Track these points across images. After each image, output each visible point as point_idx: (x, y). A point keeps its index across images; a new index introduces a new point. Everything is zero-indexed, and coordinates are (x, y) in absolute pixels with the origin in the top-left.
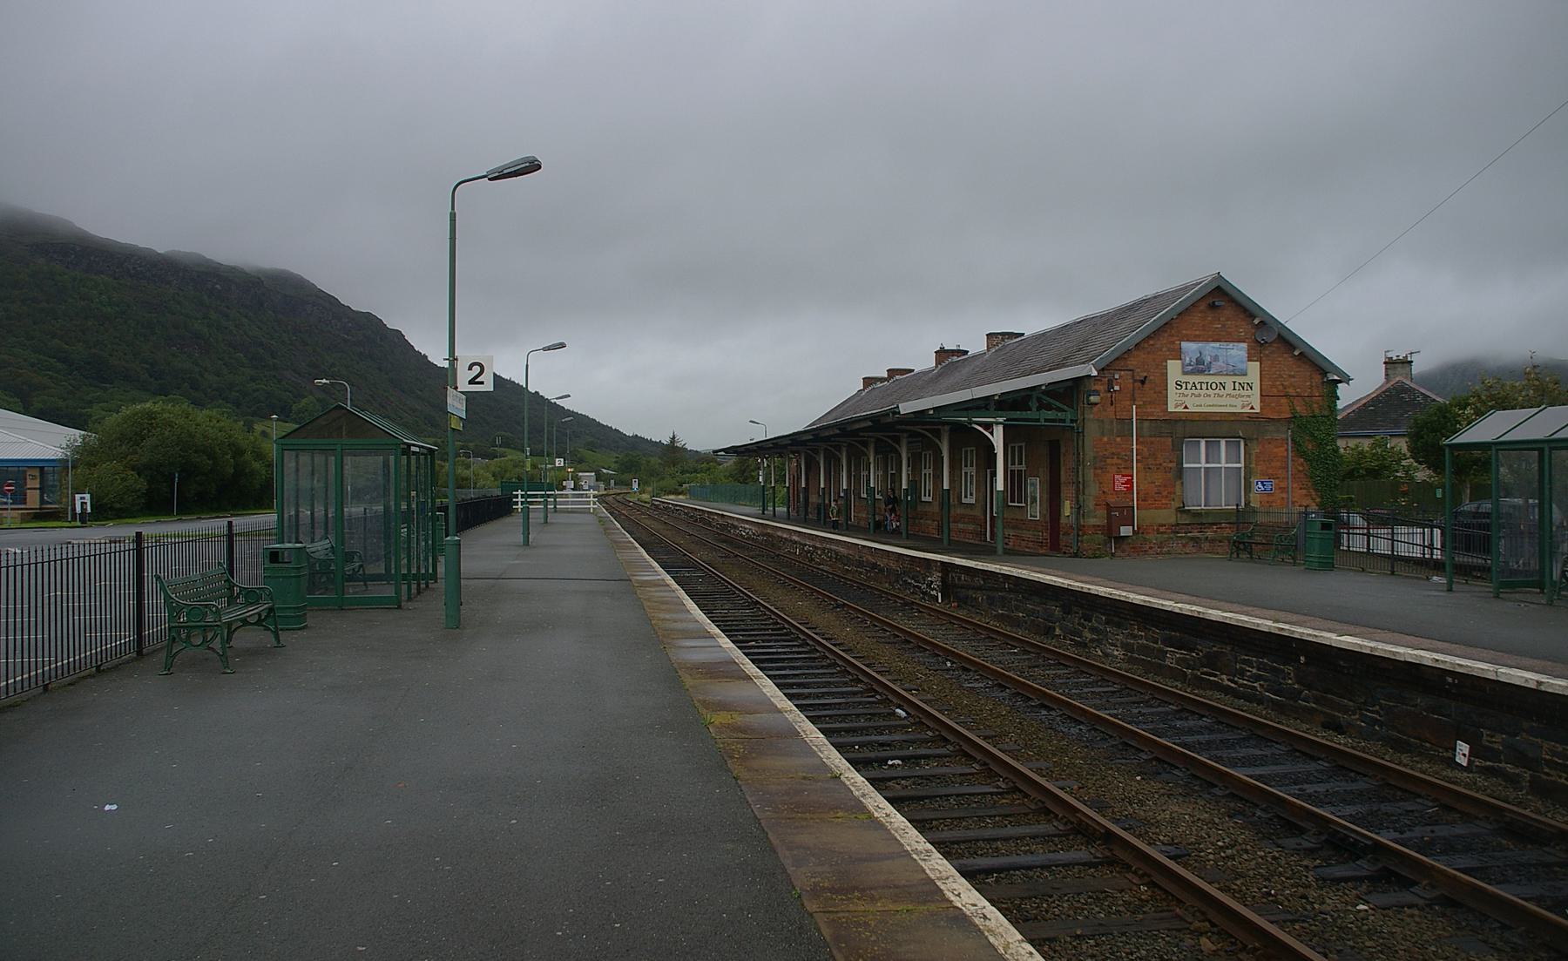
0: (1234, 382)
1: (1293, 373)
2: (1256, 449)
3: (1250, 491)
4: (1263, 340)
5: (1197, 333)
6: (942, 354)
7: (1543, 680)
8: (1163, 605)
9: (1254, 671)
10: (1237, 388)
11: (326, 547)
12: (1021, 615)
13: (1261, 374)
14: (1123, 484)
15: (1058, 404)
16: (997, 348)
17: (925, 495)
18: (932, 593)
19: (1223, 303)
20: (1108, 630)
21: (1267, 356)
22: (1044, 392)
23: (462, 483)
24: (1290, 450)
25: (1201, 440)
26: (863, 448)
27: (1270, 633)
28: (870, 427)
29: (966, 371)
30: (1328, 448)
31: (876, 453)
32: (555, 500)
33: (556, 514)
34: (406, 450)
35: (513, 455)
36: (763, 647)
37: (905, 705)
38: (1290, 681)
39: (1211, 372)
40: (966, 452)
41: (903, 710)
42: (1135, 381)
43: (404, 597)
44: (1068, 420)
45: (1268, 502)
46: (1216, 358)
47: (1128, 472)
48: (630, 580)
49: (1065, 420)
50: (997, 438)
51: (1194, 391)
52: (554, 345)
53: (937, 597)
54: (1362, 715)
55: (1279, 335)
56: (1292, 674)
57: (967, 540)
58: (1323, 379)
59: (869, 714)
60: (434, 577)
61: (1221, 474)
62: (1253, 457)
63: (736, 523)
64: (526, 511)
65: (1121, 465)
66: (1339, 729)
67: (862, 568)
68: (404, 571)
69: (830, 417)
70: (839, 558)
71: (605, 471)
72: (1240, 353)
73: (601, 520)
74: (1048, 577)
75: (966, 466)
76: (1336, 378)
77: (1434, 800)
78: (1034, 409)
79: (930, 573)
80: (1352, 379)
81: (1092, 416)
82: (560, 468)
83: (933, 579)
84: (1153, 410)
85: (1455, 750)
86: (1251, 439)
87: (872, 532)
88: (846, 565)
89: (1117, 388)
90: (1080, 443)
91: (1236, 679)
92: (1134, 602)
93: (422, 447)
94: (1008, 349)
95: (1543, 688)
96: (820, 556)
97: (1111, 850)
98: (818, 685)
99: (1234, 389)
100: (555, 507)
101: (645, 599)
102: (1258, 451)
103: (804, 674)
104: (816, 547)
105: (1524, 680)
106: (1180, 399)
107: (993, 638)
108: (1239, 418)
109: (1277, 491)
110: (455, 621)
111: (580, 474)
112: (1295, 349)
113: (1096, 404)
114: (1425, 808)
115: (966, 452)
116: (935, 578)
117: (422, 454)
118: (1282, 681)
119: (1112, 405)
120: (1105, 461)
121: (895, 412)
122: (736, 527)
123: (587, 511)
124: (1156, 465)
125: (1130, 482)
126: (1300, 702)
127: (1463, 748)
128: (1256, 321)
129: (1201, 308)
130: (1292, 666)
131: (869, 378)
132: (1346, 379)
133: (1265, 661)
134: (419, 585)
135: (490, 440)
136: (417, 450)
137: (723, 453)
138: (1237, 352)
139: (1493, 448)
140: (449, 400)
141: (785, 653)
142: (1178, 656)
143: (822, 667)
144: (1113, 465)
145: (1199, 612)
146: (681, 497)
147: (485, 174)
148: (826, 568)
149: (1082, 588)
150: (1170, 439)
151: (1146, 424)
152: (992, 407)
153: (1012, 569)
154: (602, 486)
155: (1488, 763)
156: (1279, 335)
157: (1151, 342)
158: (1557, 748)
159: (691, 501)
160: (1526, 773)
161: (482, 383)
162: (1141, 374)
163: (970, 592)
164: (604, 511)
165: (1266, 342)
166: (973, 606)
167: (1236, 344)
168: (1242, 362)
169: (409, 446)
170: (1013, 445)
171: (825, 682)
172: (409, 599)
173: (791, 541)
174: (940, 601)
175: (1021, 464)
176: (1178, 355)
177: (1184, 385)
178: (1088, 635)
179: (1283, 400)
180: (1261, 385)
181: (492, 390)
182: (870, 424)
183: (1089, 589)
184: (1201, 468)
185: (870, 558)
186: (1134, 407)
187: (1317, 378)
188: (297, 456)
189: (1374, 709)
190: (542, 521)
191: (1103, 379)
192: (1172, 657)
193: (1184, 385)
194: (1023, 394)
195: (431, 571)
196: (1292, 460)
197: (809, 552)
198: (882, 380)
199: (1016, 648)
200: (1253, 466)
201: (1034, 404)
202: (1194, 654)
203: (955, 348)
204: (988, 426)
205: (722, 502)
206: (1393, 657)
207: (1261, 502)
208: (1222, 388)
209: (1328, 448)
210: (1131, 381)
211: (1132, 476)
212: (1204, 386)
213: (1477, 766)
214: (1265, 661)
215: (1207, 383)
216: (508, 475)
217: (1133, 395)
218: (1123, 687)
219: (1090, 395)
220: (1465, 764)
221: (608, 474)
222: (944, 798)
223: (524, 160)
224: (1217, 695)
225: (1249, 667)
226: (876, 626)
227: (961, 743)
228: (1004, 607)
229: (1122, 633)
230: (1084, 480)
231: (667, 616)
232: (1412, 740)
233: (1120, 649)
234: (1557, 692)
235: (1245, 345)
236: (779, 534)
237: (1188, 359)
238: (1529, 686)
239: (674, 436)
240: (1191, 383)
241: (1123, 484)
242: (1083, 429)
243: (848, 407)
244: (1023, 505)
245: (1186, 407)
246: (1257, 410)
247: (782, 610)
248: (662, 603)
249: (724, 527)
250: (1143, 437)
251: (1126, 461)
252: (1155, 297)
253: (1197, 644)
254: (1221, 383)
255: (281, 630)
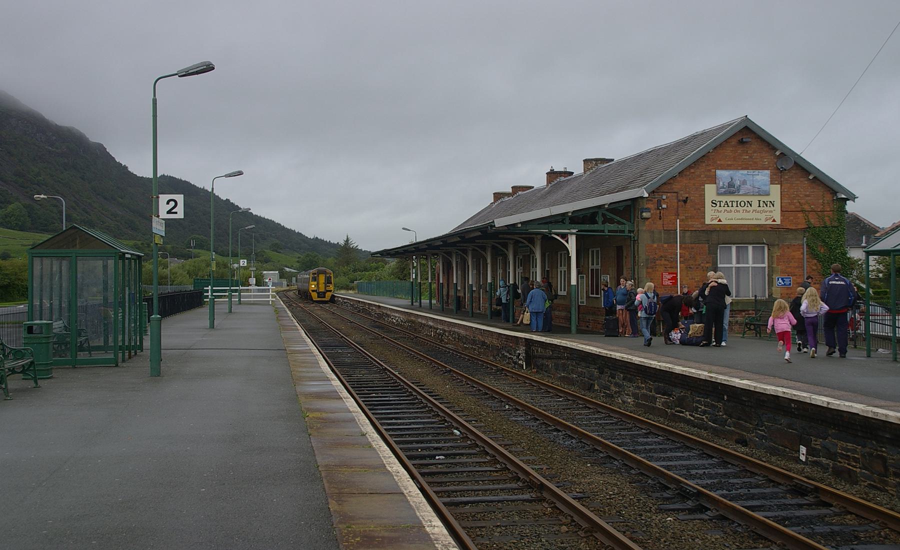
0: (759, 201)
1: (808, 193)
2: (777, 252)
3: (772, 286)
4: (782, 168)
5: (729, 163)
6: (552, 175)
7: (830, 401)
8: (651, 364)
9: (703, 408)
10: (761, 205)
11: (60, 326)
12: (575, 376)
13: (781, 194)
14: (669, 280)
15: (618, 218)
16: (591, 171)
17: (561, 290)
18: (519, 362)
19: (750, 140)
20: (625, 384)
21: (787, 180)
22: (607, 210)
23: (162, 280)
24: (805, 254)
25: (732, 245)
26: (482, 252)
27: (706, 380)
28: (480, 236)
29: (566, 189)
30: (837, 251)
31: (473, 258)
32: (240, 295)
33: (240, 306)
34: (122, 256)
35: (204, 255)
36: (381, 397)
37: (461, 428)
38: (721, 414)
39: (740, 193)
40: (561, 254)
41: (459, 431)
42: (679, 201)
43: (120, 360)
44: (626, 231)
45: (787, 294)
46: (744, 182)
47: (673, 271)
48: (286, 350)
49: (624, 231)
50: (572, 245)
51: (726, 208)
52: (235, 173)
53: (523, 365)
54: (756, 433)
55: (795, 163)
56: (722, 409)
57: (561, 324)
58: (833, 197)
59: (436, 433)
60: (141, 348)
61: (749, 273)
62: (775, 259)
63: (389, 313)
64: (213, 303)
65: (667, 265)
66: (743, 442)
67: (475, 345)
68: (120, 344)
69: (470, 223)
70: (460, 338)
71: (287, 269)
72: (764, 178)
73: (277, 311)
74: (588, 347)
75: (561, 266)
76: (843, 196)
77: (764, 477)
78: (600, 223)
79: (518, 347)
80: (857, 197)
81: (644, 228)
82: (244, 268)
83: (520, 352)
84: (694, 223)
85: (799, 452)
86: (773, 245)
87: (489, 319)
88: (465, 343)
89: (664, 206)
90: (636, 249)
91: (694, 414)
92: (635, 362)
93: (133, 254)
94: (598, 172)
95: (830, 406)
96: (448, 337)
97: (542, 493)
98: (409, 418)
99: (759, 206)
100: (240, 300)
101: (291, 361)
102: (779, 254)
103: (402, 412)
104: (445, 331)
105: (821, 402)
106: (714, 214)
107: (549, 392)
108: (763, 229)
109: (795, 286)
110: (156, 372)
111: (265, 272)
112: (810, 174)
113: (649, 219)
114: (758, 481)
115: (561, 254)
116: (521, 350)
117: (133, 259)
118: (717, 414)
119: (660, 219)
120: (655, 263)
121: (492, 225)
122: (388, 316)
123: (266, 303)
124: (696, 265)
125: (675, 278)
126: (726, 427)
127: (803, 449)
128: (778, 153)
129: (733, 143)
130: (722, 403)
131: (499, 193)
132: (853, 198)
133: (708, 400)
134: (130, 352)
135: (186, 242)
136: (129, 256)
137: (379, 255)
138: (762, 177)
139: (892, 254)
140: (154, 225)
141: (394, 400)
142: (663, 400)
143: (417, 408)
144: (661, 265)
145: (669, 368)
146: (351, 292)
147: (176, 72)
148: (450, 346)
149: (607, 354)
150: (707, 245)
151: (688, 234)
152: (567, 221)
153: (568, 343)
154: (285, 282)
155: (815, 458)
156: (795, 163)
157: (692, 171)
158: (843, 445)
159: (358, 295)
160: (830, 462)
161: (176, 213)
162: (683, 195)
163: (545, 362)
164: (282, 303)
165: (785, 170)
166: (546, 372)
167: (760, 171)
168: (766, 185)
169: (124, 254)
170: (593, 249)
171: (415, 416)
172: (123, 361)
173: (427, 326)
174: (524, 368)
175: (598, 265)
176: (713, 180)
177: (718, 204)
178: (613, 388)
179: (800, 215)
180: (781, 203)
181: (183, 217)
182: (480, 233)
183: (611, 355)
184: (749, 267)
185: (480, 337)
186: (678, 220)
187: (828, 197)
188: (42, 261)
189: (762, 428)
190: (228, 311)
191: (653, 200)
192: (660, 401)
193: (718, 204)
194: (591, 211)
195: (138, 344)
196: (808, 262)
197: (439, 334)
198: (508, 195)
199: (561, 397)
200: (774, 266)
201: (600, 219)
202: (671, 398)
203: (563, 170)
204: (564, 236)
205: (383, 296)
206: (764, 392)
207: (781, 294)
208: (749, 205)
209: (837, 251)
210: (676, 201)
211: (676, 274)
212: (735, 204)
213: (810, 461)
214: (708, 400)
215: (737, 202)
216: (200, 273)
217: (677, 212)
218: (620, 420)
219: (643, 212)
220: (804, 460)
221: (290, 272)
222: (460, 473)
223: (203, 64)
224: (687, 428)
225: (700, 405)
226: (469, 384)
227: (485, 446)
228: (564, 371)
229: (633, 386)
230: (638, 277)
231: (304, 370)
232: (780, 447)
233: (631, 398)
234: (835, 408)
235: (768, 172)
236: (420, 320)
237: (721, 183)
238: (824, 406)
239: (348, 239)
240: (724, 202)
241: (669, 280)
242: (638, 238)
243: (480, 217)
244: (599, 296)
245: (720, 221)
246: (778, 222)
247: (404, 375)
248: (304, 363)
249: (381, 316)
250: (685, 243)
251: (672, 262)
252: (702, 134)
253: (672, 391)
254: (748, 202)
255: (39, 379)
